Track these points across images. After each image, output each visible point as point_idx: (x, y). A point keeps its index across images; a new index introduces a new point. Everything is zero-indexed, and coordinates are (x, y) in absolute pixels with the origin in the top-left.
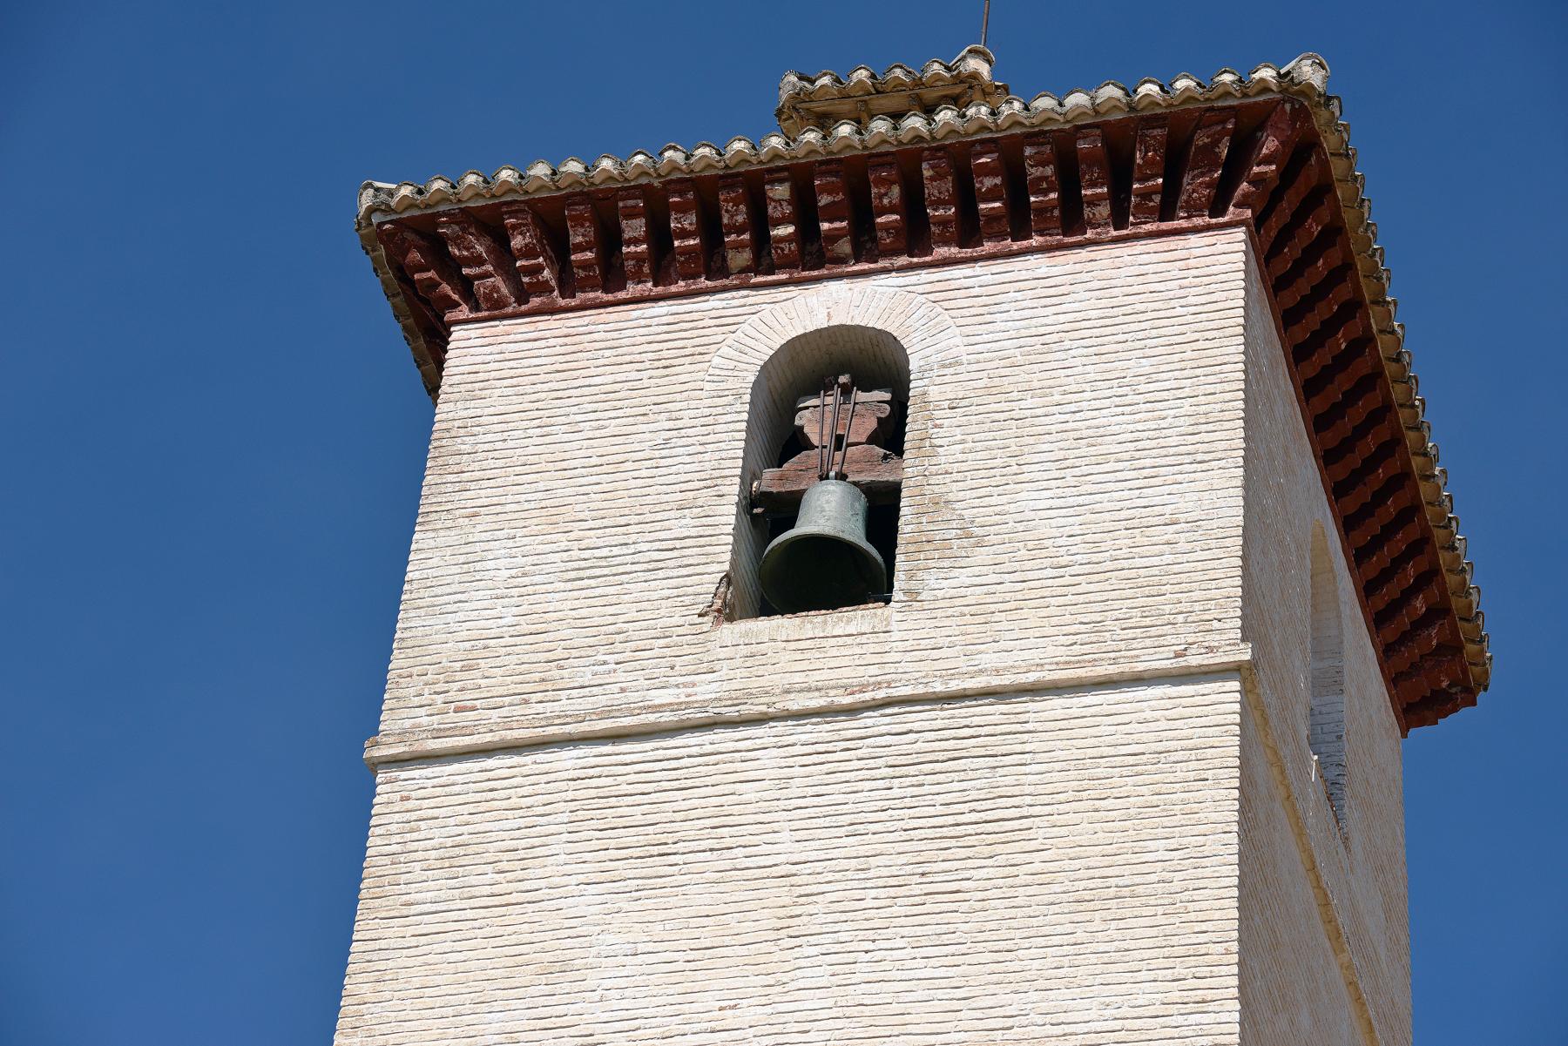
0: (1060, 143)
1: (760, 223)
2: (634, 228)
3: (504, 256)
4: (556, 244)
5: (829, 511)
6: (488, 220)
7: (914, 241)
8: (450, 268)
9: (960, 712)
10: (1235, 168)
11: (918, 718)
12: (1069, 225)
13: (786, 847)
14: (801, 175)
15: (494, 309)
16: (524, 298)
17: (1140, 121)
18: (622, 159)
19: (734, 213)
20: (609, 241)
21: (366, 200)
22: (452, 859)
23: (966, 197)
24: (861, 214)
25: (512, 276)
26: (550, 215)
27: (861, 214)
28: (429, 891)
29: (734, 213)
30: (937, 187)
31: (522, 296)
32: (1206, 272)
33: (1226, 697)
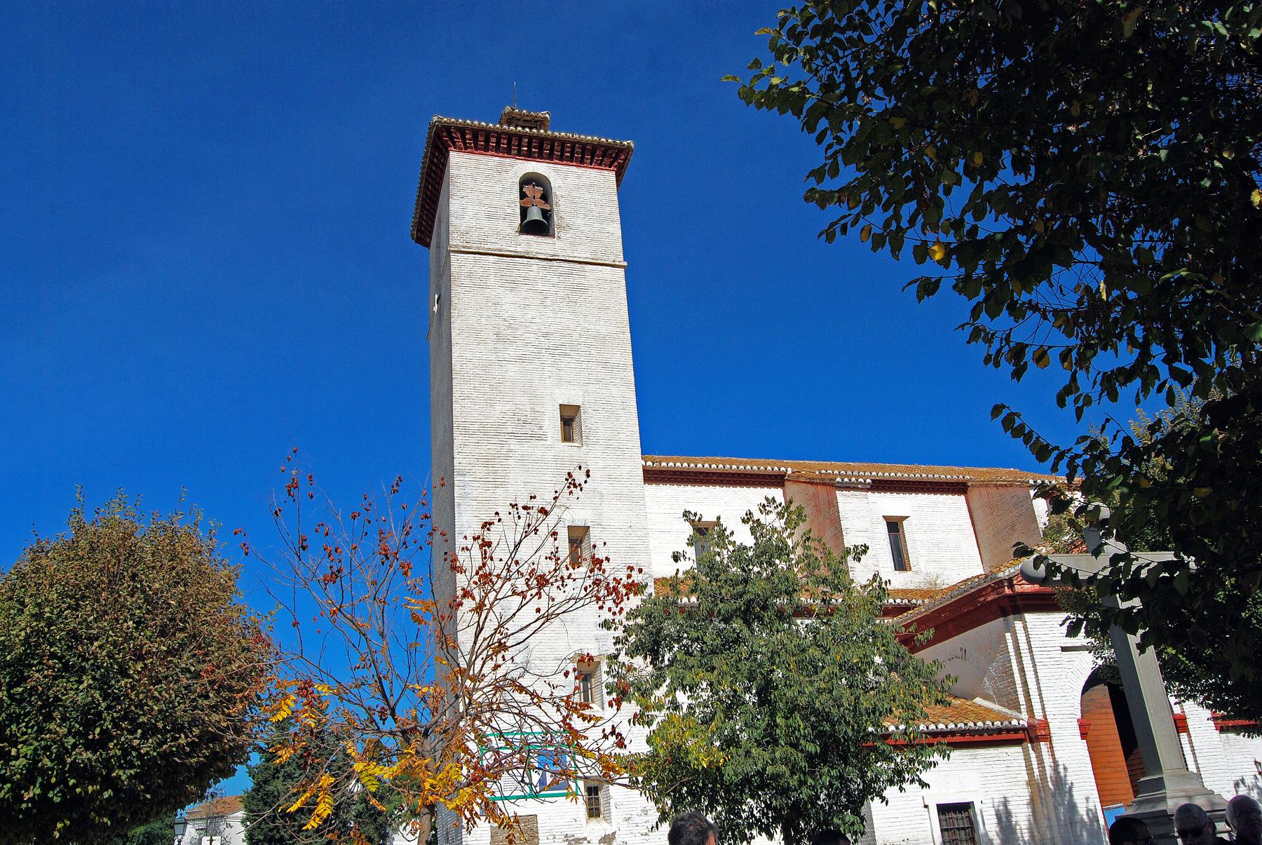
0: (584, 145)
1: (520, 146)
2: (494, 140)
3: (464, 139)
4: (475, 138)
5: (535, 214)
6: (462, 131)
7: (550, 158)
8: (452, 139)
9: (572, 265)
10: (615, 159)
11: (563, 264)
12: (581, 162)
13: (540, 287)
14: (531, 138)
15: (460, 150)
16: (465, 148)
17: (600, 145)
18: (472, 121)
19: (515, 142)
20: (487, 141)
21: (435, 119)
22: (470, 275)
23: (562, 151)
24: (541, 149)
25: (465, 144)
26: (476, 132)
27: (541, 149)
28: (467, 282)
29: (515, 142)
30: (557, 147)
31: (466, 148)
32: (459, 162)
33: (621, 272)
